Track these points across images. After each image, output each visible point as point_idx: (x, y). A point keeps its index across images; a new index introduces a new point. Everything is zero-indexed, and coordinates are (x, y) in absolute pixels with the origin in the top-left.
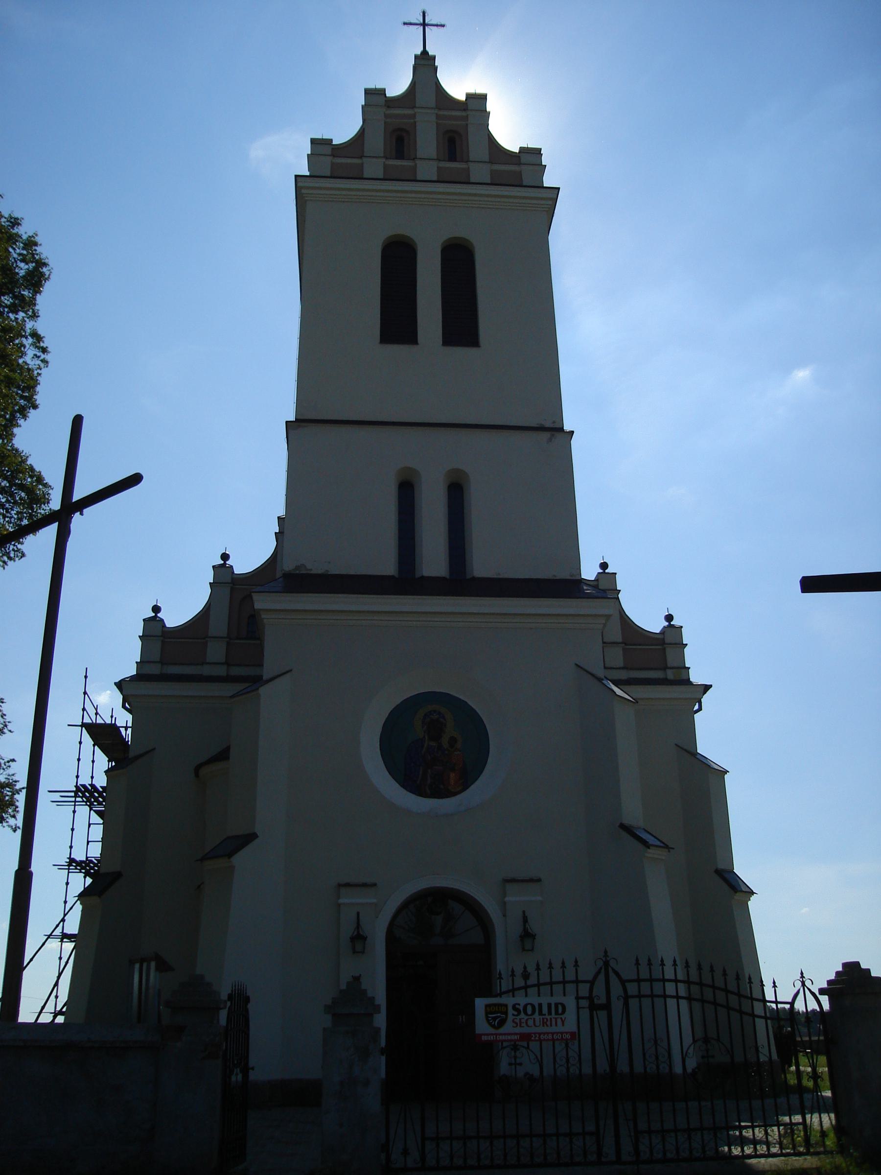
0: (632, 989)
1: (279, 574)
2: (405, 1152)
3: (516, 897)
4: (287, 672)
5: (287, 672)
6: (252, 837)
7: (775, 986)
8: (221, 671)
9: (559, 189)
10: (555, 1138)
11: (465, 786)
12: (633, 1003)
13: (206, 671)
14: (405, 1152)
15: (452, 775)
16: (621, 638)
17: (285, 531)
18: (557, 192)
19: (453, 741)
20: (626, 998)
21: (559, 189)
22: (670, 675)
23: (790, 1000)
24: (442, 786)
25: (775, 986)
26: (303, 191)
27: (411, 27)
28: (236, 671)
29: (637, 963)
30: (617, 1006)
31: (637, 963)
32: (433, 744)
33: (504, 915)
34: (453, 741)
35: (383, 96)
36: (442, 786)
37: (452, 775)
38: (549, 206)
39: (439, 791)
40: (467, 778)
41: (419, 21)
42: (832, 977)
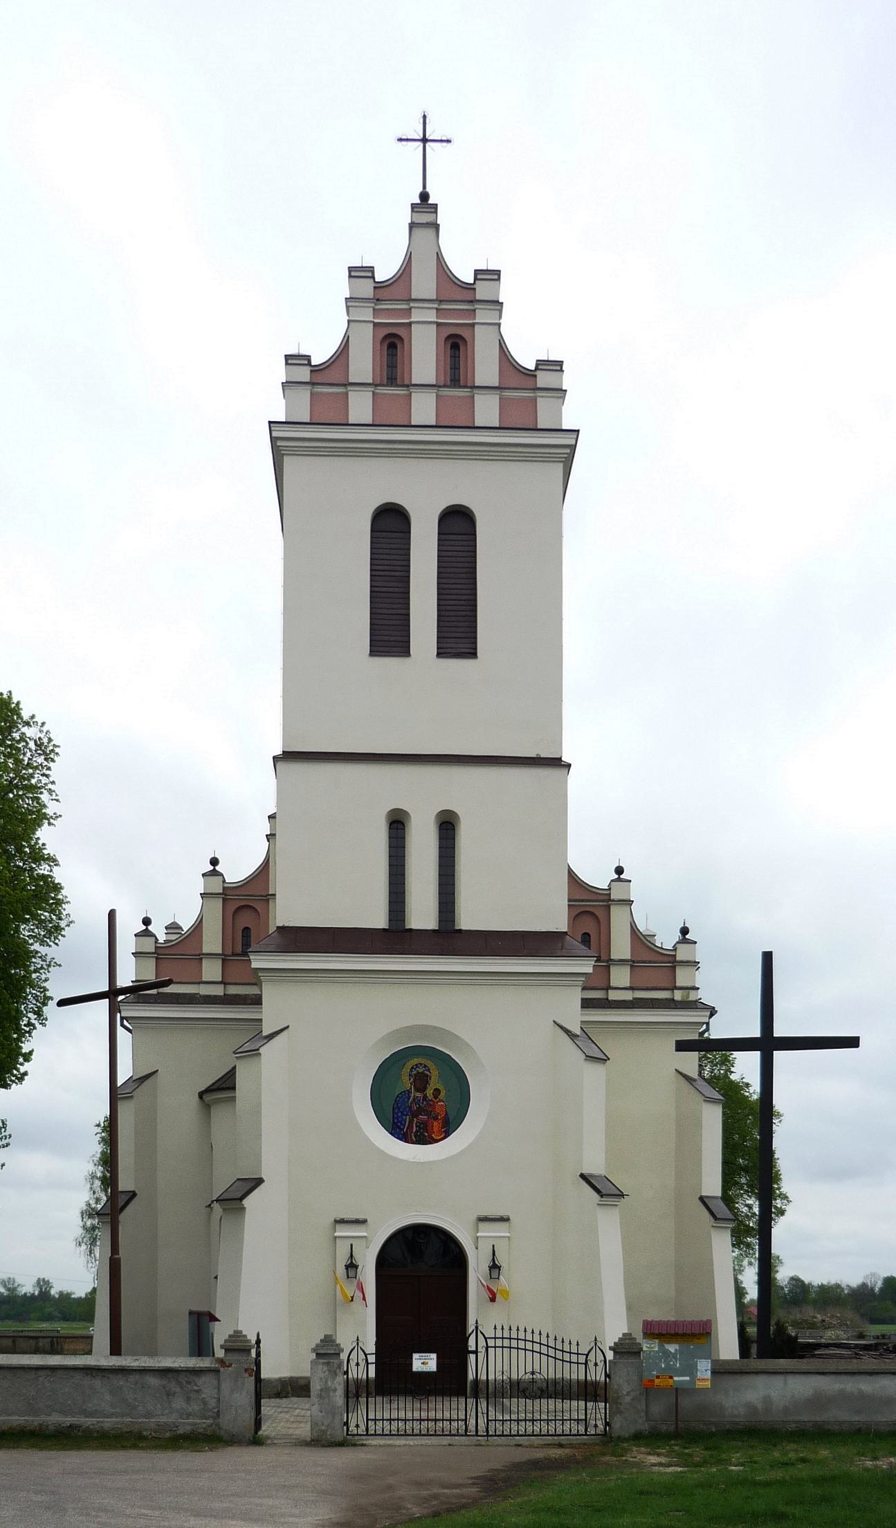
0: (491, 1343)
1: (272, 929)
2: (357, 1426)
3: (487, 1231)
4: (282, 1030)
5: (282, 1030)
6: (259, 1181)
7: (578, 1344)
8: (218, 991)
9: (578, 431)
10: (411, 1422)
11: (447, 1134)
12: (491, 1351)
13: (204, 990)
14: (357, 1426)
15: (435, 1124)
16: (630, 955)
17: (277, 893)
18: (576, 437)
19: (437, 1091)
20: (487, 1347)
21: (578, 431)
22: (678, 995)
23: (586, 1353)
24: (426, 1134)
25: (578, 1344)
26: (279, 443)
27: (410, 143)
28: (233, 990)
29: (495, 1328)
30: (481, 1350)
31: (495, 1328)
32: (418, 1094)
33: (477, 1248)
34: (437, 1091)
35: (372, 280)
36: (426, 1134)
37: (435, 1124)
38: (566, 456)
39: (424, 1138)
40: (449, 1127)
41: (419, 135)
42: (617, 1340)
